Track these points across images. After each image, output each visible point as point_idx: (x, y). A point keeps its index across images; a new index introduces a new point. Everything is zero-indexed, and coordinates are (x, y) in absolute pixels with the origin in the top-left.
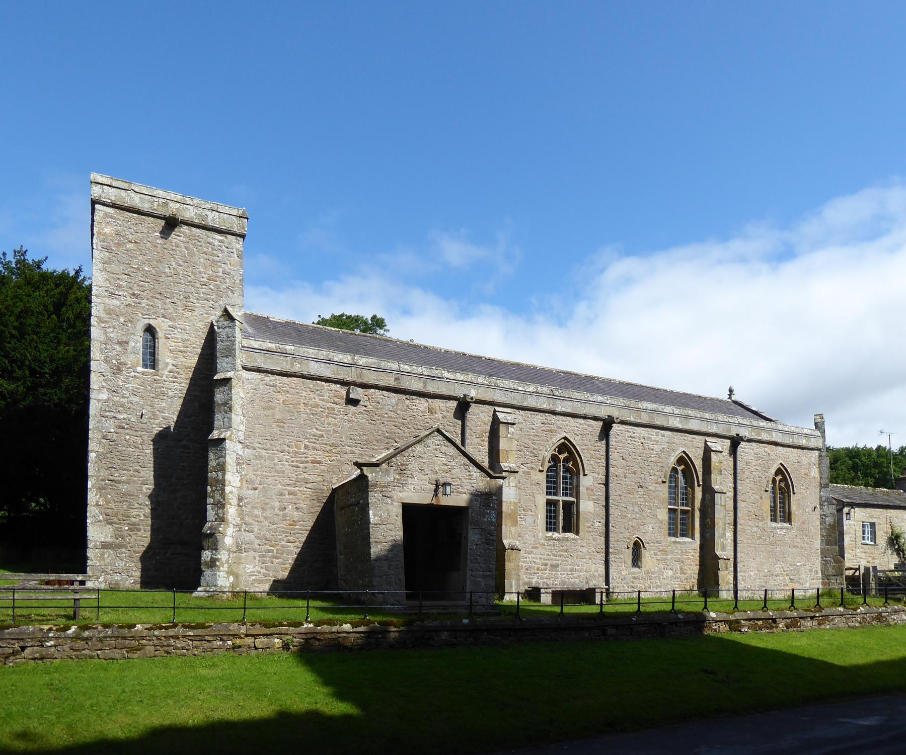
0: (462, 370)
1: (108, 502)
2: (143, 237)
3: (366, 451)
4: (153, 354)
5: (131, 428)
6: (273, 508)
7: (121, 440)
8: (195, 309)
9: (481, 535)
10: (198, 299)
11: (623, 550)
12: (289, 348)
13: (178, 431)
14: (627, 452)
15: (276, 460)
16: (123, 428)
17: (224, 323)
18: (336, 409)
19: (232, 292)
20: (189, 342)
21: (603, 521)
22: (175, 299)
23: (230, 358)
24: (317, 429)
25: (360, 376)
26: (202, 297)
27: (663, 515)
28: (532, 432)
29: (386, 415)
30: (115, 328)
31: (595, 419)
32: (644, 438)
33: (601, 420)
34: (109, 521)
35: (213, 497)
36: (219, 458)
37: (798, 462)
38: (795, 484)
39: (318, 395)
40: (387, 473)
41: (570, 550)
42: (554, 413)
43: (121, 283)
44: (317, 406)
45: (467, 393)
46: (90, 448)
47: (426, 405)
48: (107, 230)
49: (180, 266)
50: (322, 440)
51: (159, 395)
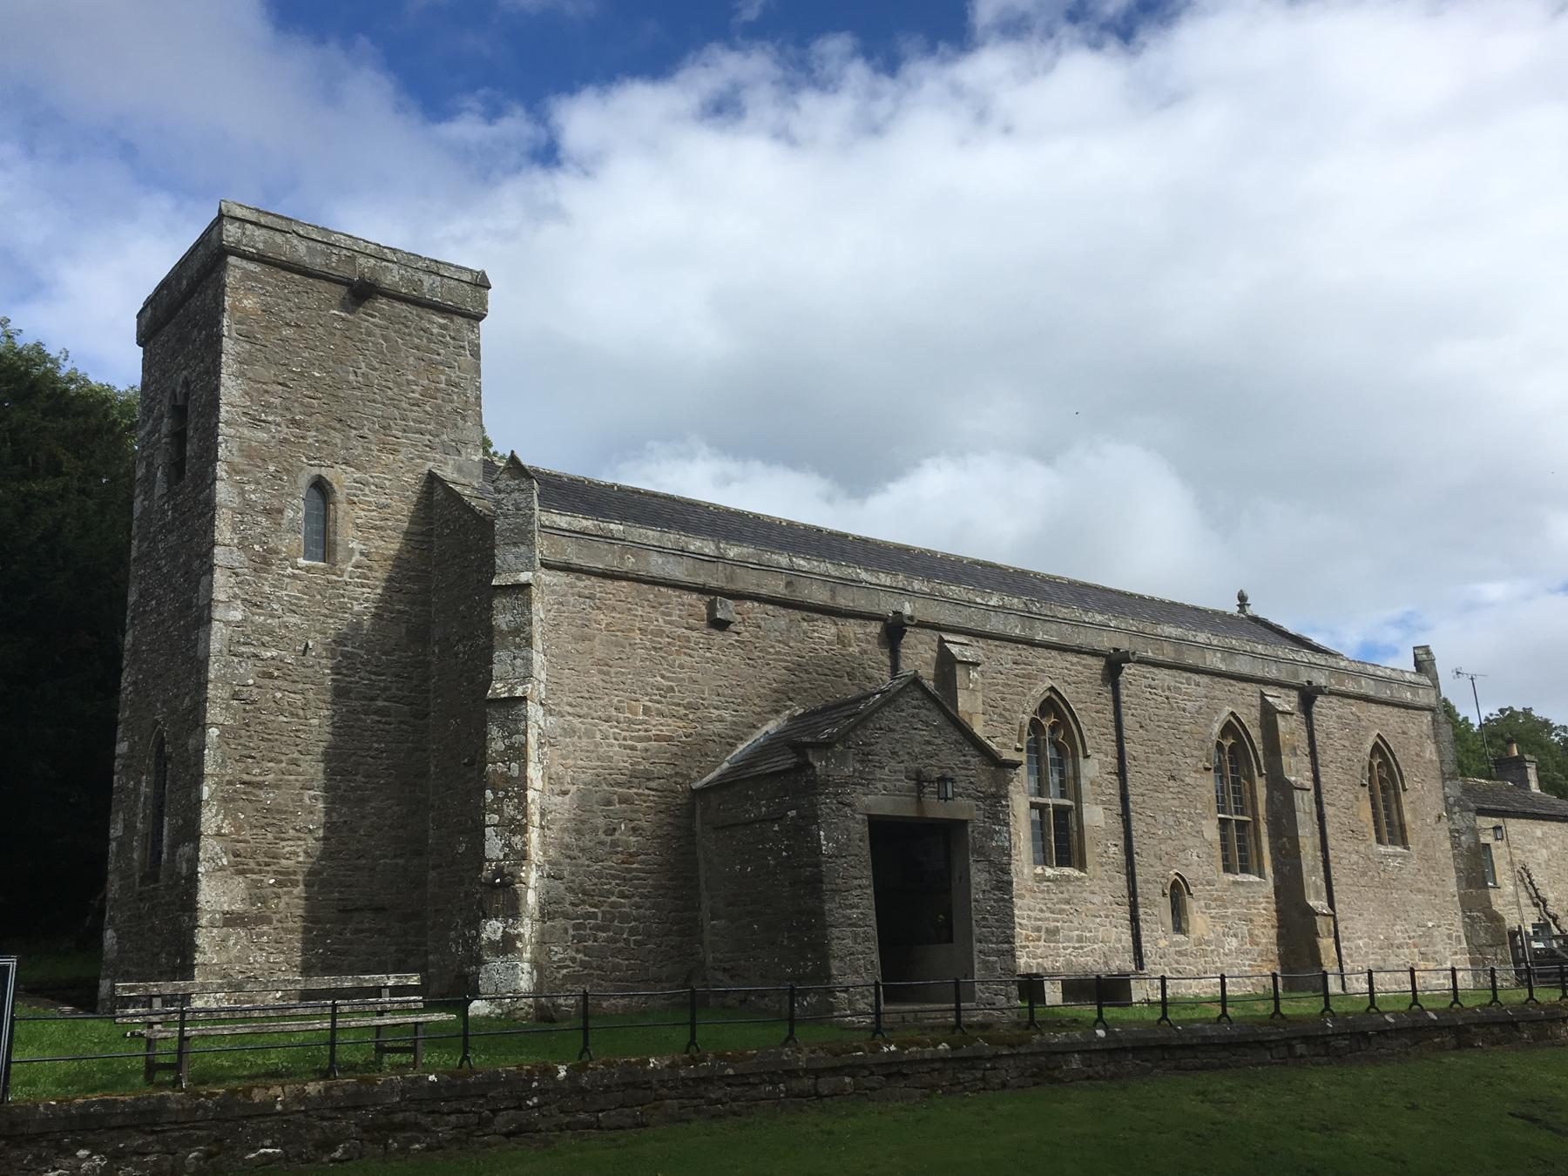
0: (890, 569)
2: (310, 316)
4: (325, 532)
5: (284, 677)
6: (595, 830)
7: (267, 700)
8: (400, 449)
9: (989, 872)
10: (405, 431)
11: (1158, 898)
12: (616, 527)
13: (370, 680)
14: (1147, 714)
15: (598, 736)
16: (271, 676)
19: (464, 418)
20: (389, 511)
21: (1121, 843)
22: (366, 428)
24: (663, 677)
26: (411, 427)
27: (1212, 832)
28: (1001, 679)
29: (771, 650)
30: (260, 484)
31: (1094, 653)
32: (1169, 689)
33: (1104, 656)
34: (240, 867)
36: (510, 736)
37: (1404, 733)
38: (1404, 773)
39: (663, 614)
40: (842, 758)
41: (1075, 901)
42: (1032, 643)
43: (272, 400)
44: (660, 633)
45: (899, 609)
46: (210, 718)
47: (834, 630)
48: (248, 303)
49: (375, 369)
50: (671, 697)
51: (337, 611)
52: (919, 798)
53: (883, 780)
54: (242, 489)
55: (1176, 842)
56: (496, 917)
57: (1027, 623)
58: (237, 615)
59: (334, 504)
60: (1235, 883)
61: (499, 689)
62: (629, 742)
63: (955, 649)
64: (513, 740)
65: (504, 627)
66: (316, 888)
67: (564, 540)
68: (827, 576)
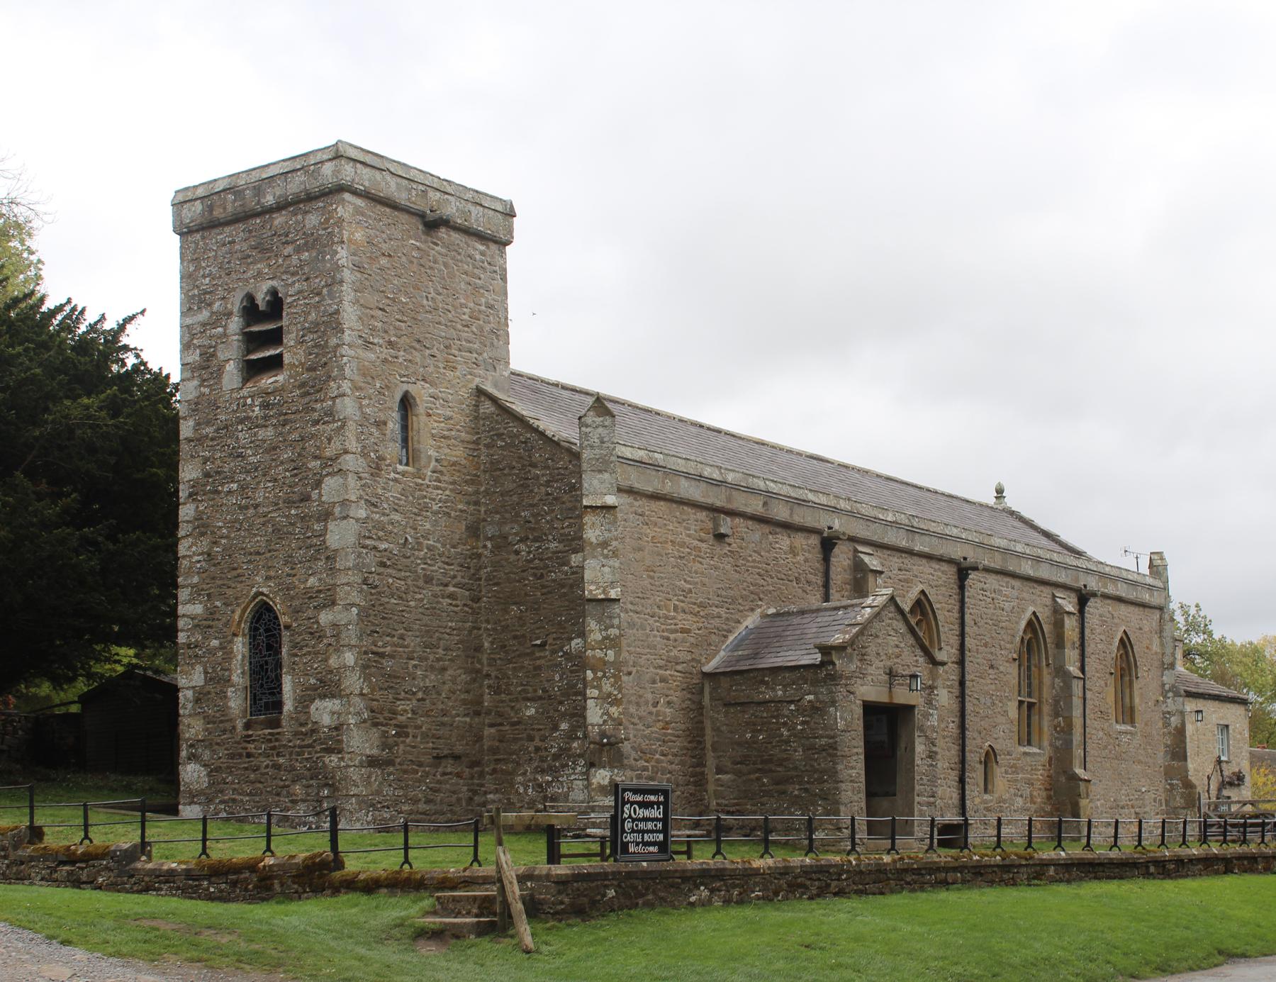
1: (373, 690)
3: (731, 613)
5: (393, 566)
6: (647, 703)
8: (457, 366)
9: (925, 744)
13: (444, 569)
17: (594, 419)
18: (703, 550)
19: (497, 336)
23: (605, 474)
24: (685, 581)
25: (729, 499)
29: (750, 559)
31: (950, 561)
35: (599, 687)
36: (606, 629)
37: (1140, 629)
43: (376, 324)
44: (683, 545)
49: (439, 294)
52: (890, 688)
53: (872, 675)
54: (361, 403)
55: (990, 720)
56: (604, 767)
57: (910, 536)
58: (362, 513)
59: (416, 416)
60: (1025, 754)
61: (592, 590)
62: (666, 634)
63: (866, 559)
64: (609, 633)
65: (594, 540)
66: (419, 739)
67: (629, 468)
68: (789, 497)
